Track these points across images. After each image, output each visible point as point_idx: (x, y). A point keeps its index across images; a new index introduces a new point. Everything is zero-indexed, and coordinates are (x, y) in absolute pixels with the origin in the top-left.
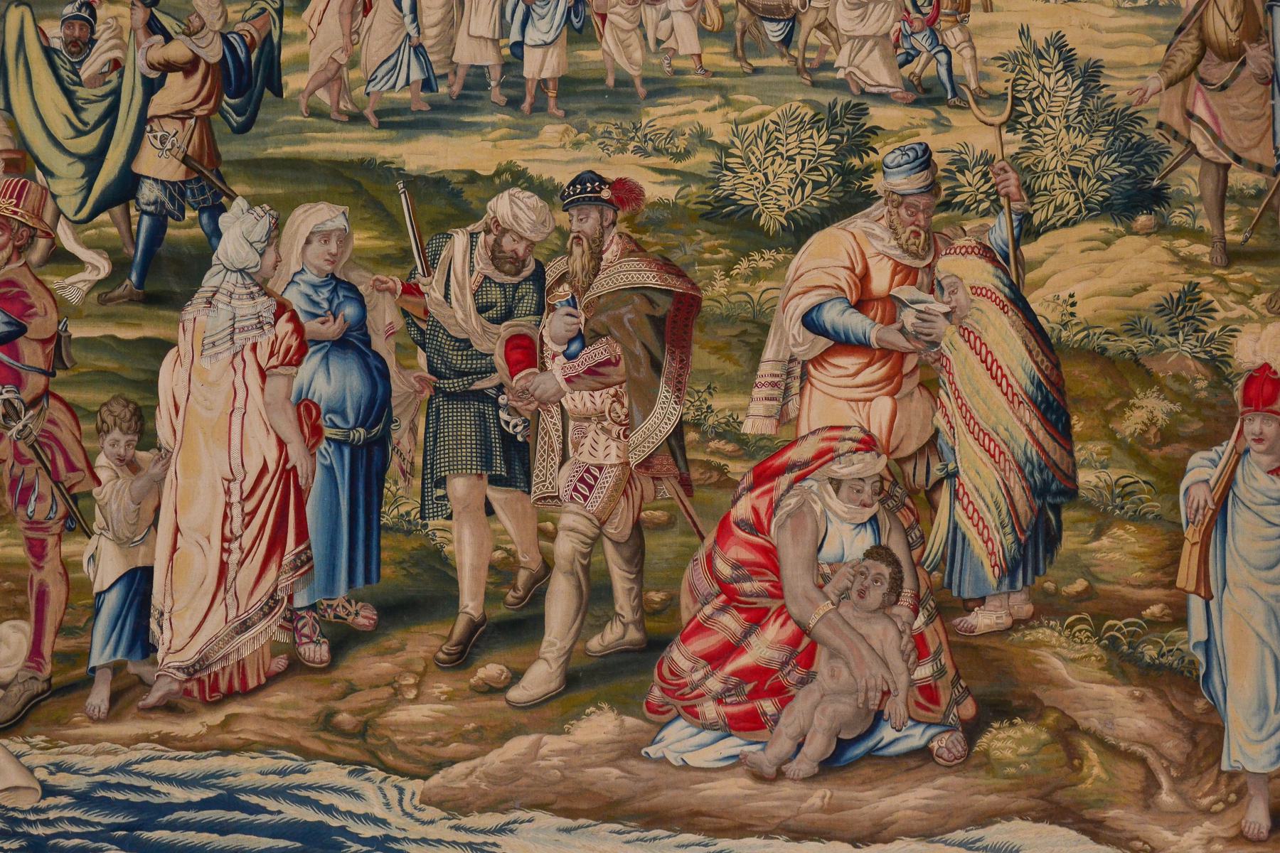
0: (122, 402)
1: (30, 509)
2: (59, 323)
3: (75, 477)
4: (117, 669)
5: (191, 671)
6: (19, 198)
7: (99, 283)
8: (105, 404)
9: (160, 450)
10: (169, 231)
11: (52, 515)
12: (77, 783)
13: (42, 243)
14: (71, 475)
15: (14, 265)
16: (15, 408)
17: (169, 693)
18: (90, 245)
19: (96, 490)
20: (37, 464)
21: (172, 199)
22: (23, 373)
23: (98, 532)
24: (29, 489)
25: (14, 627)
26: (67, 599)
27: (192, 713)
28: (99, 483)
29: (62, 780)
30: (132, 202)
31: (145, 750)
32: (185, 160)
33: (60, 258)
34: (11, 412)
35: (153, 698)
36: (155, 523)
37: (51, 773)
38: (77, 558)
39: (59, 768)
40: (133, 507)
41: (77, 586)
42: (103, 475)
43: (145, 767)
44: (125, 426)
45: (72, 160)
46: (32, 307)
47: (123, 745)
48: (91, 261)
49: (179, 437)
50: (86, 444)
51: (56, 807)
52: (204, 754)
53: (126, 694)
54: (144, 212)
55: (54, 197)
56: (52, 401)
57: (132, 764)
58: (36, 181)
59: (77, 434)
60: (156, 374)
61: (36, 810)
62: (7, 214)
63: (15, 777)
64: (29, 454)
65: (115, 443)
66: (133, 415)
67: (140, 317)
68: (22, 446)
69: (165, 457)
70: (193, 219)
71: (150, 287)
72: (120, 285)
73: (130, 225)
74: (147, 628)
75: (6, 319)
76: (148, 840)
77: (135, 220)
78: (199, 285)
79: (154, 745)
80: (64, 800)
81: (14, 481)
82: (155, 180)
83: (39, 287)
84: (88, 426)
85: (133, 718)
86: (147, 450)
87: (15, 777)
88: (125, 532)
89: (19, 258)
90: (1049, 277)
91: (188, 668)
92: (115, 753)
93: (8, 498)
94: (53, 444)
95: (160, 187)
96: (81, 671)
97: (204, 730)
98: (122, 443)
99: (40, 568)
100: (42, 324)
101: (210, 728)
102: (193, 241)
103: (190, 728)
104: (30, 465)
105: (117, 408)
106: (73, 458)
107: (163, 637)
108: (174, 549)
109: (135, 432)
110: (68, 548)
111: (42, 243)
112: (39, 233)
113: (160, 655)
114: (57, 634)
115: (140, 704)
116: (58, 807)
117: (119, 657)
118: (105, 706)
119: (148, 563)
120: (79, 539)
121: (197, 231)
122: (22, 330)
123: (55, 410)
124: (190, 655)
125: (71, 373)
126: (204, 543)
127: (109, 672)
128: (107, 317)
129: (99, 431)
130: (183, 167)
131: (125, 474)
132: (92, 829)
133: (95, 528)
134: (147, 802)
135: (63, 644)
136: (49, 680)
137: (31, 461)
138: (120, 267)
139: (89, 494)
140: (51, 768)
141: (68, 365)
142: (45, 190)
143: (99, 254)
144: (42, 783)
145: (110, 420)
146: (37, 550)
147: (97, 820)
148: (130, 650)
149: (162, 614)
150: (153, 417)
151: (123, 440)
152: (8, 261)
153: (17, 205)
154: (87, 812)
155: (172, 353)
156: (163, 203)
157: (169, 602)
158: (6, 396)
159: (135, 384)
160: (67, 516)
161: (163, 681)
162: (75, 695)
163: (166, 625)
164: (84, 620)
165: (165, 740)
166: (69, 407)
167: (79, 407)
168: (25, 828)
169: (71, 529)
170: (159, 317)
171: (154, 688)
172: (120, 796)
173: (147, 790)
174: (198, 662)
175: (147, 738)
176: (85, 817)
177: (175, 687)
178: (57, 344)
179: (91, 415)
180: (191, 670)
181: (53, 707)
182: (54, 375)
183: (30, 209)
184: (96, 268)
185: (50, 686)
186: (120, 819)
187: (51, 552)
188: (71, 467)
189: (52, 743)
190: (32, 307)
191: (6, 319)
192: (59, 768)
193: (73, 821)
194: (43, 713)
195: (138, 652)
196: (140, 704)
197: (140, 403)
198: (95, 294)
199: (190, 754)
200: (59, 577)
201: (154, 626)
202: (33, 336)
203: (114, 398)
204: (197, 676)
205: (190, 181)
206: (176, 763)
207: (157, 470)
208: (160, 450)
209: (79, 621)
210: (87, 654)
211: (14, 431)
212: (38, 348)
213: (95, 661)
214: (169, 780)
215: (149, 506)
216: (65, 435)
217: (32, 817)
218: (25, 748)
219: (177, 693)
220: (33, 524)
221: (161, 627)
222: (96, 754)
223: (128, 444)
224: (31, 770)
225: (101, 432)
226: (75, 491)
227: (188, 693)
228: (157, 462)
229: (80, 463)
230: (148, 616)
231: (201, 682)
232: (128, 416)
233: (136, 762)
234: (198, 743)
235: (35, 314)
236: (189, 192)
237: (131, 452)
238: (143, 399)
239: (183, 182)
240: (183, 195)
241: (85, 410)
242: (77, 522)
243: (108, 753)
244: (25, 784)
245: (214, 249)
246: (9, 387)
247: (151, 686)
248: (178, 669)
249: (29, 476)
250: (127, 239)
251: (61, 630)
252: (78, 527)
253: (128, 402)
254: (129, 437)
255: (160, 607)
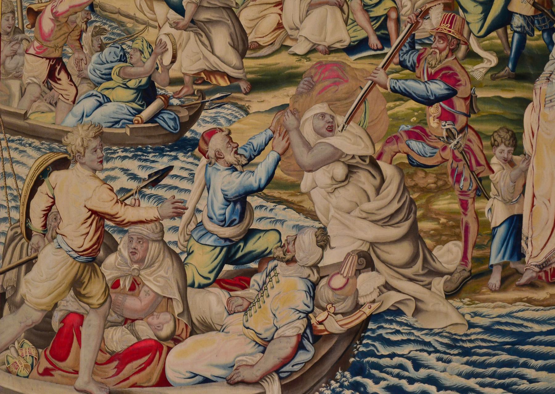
0: (505, 130)
1: (461, 185)
2: (471, 89)
3: (479, 169)
4: (504, 266)
5: (542, 267)
6: (451, 23)
7: (491, 69)
8: (496, 132)
9: (525, 155)
10: (528, 42)
11: (470, 188)
12: (485, 322)
13: (463, 48)
14: (478, 168)
15: (450, 59)
16: (452, 133)
17: (532, 278)
18: (486, 49)
19: (491, 176)
20: (464, 162)
21: (528, 25)
22: (456, 115)
23: (493, 196)
24: (460, 175)
25: (454, 244)
26: (478, 231)
27: (542, 288)
28: (493, 172)
29: (477, 320)
30: (509, 26)
31: (520, 306)
32: (534, 5)
33: (471, 55)
34: (451, 135)
35: (523, 280)
36: (523, 193)
37: (472, 317)
38: (482, 210)
39: (476, 314)
40: (512, 184)
41: (483, 225)
42: (495, 168)
43: (520, 314)
44: (507, 143)
45: (476, 4)
46: (459, 81)
47: (509, 303)
48: (487, 57)
49: (534, 149)
50: (485, 152)
51: (474, 333)
52: (548, 308)
53: (509, 278)
54: (515, 32)
55: (468, 23)
56: (469, 130)
57: (513, 313)
58: (459, 15)
59: (481, 147)
60: (522, 116)
61: (466, 335)
62: (446, 32)
63: (456, 319)
64: (460, 156)
65: (502, 152)
66: (511, 137)
67: (514, 87)
68: (456, 152)
69: (528, 159)
70: (538, 35)
71: (519, 71)
72: (503, 70)
73: (507, 38)
74: (520, 245)
75: (447, 87)
76: (522, 350)
77: (510, 36)
78: (543, 70)
79: (525, 304)
80: (478, 330)
81: (453, 171)
82: (520, 15)
83: (463, 71)
84: (486, 143)
85: (513, 290)
86: (519, 155)
87: (456, 319)
88: (508, 197)
89: (452, 55)
90: (266, 111)
91: (540, 265)
92: (504, 307)
93: (450, 179)
94: (470, 152)
95: (522, 18)
96: (485, 267)
97: (548, 296)
98: (506, 152)
99: (466, 215)
100: (463, 91)
101: (551, 295)
102: (538, 47)
103: (541, 295)
104: (461, 162)
105: (503, 134)
106: (479, 159)
107: (528, 250)
108: (533, 206)
109: (512, 146)
110: (478, 205)
111: (463, 48)
112: (462, 42)
113: (526, 259)
114: (474, 247)
115: (517, 283)
116: (476, 334)
117: (506, 259)
118: (498, 284)
119: (520, 213)
120: (482, 200)
121: (541, 42)
122: (455, 93)
123: (471, 135)
124: (541, 259)
125: (478, 115)
126: (547, 202)
127: (500, 268)
128: (496, 87)
129: (492, 145)
130: (533, 8)
131: (507, 167)
132: (493, 345)
133: (491, 194)
134: (521, 331)
135: (477, 253)
136: (470, 271)
137: (461, 160)
138: (503, 60)
139: (487, 178)
140: (472, 314)
141: (476, 111)
142: (464, 19)
143: (491, 54)
144: (468, 322)
145: (499, 140)
146: (464, 205)
147: (495, 340)
148: (511, 257)
149: (527, 238)
150: (521, 138)
151: (506, 149)
152: (447, 57)
153: (450, 27)
154: (490, 336)
155: (530, 105)
156: (524, 27)
157: (530, 233)
158: (447, 127)
159: (512, 121)
160: (477, 189)
161: (528, 272)
162: (483, 278)
163: (529, 244)
164: (487, 241)
165: (530, 301)
166: (477, 133)
167: (482, 133)
168: (461, 344)
169: (479, 196)
170: (524, 87)
171: (524, 275)
172: (508, 328)
173: (521, 325)
174: (545, 262)
175: (521, 300)
176: (489, 338)
177: (534, 274)
178: (471, 99)
179: (488, 137)
180: (541, 266)
181: (472, 284)
182: (469, 116)
183: (457, 29)
184: (489, 61)
185: (471, 273)
186: (507, 339)
187: (470, 206)
188: (478, 164)
189: (472, 302)
190: (459, 81)
191: (447, 87)
192: (476, 314)
193: (483, 340)
194: (467, 287)
195: (516, 257)
196: (517, 283)
197: (515, 131)
198: (489, 75)
199: (542, 308)
200: (474, 219)
201: (523, 244)
202: (460, 96)
203: (501, 128)
204: (545, 269)
205: (536, 16)
206: (535, 312)
207: (523, 165)
208: (525, 155)
209: (484, 242)
210: (488, 258)
211: (452, 145)
212: (462, 101)
213: (493, 261)
214: (532, 320)
215: (521, 183)
216: (475, 147)
217: (464, 338)
218: (461, 304)
219: (536, 277)
220: (463, 193)
221: (527, 245)
222: (494, 308)
223: (509, 152)
224: (463, 315)
225: (494, 145)
226: (480, 176)
227: (540, 278)
228: (524, 161)
229: (483, 162)
230: (521, 239)
231: (546, 273)
232: (509, 137)
233: (516, 312)
234: (545, 303)
235: (461, 85)
236: (536, 22)
237: (510, 156)
238: (517, 129)
239: (533, 16)
240: (533, 23)
241: (485, 134)
242: (482, 192)
243: (501, 307)
244: (461, 322)
245: (550, 51)
246: (449, 122)
247: (522, 274)
248: (535, 266)
249: (460, 168)
250: (506, 46)
251: (475, 246)
252: (482, 195)
253: (508, 131)
254: (510, 148)
255: (526, 235)
